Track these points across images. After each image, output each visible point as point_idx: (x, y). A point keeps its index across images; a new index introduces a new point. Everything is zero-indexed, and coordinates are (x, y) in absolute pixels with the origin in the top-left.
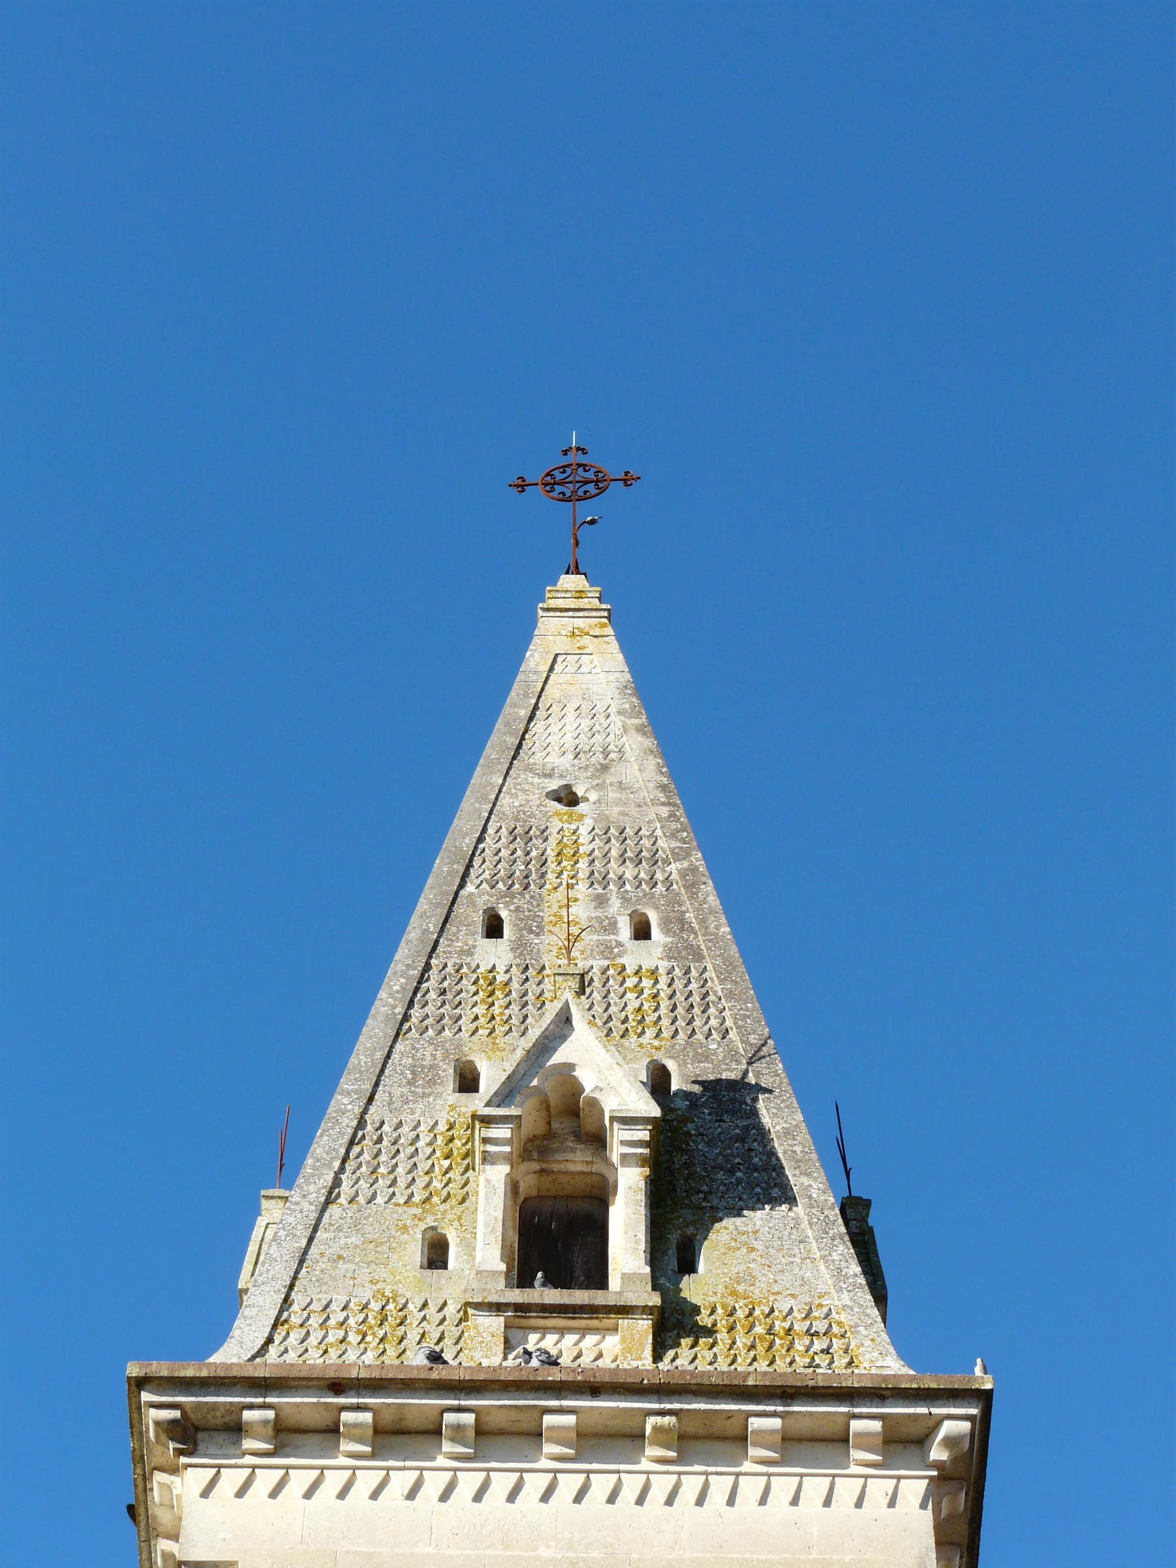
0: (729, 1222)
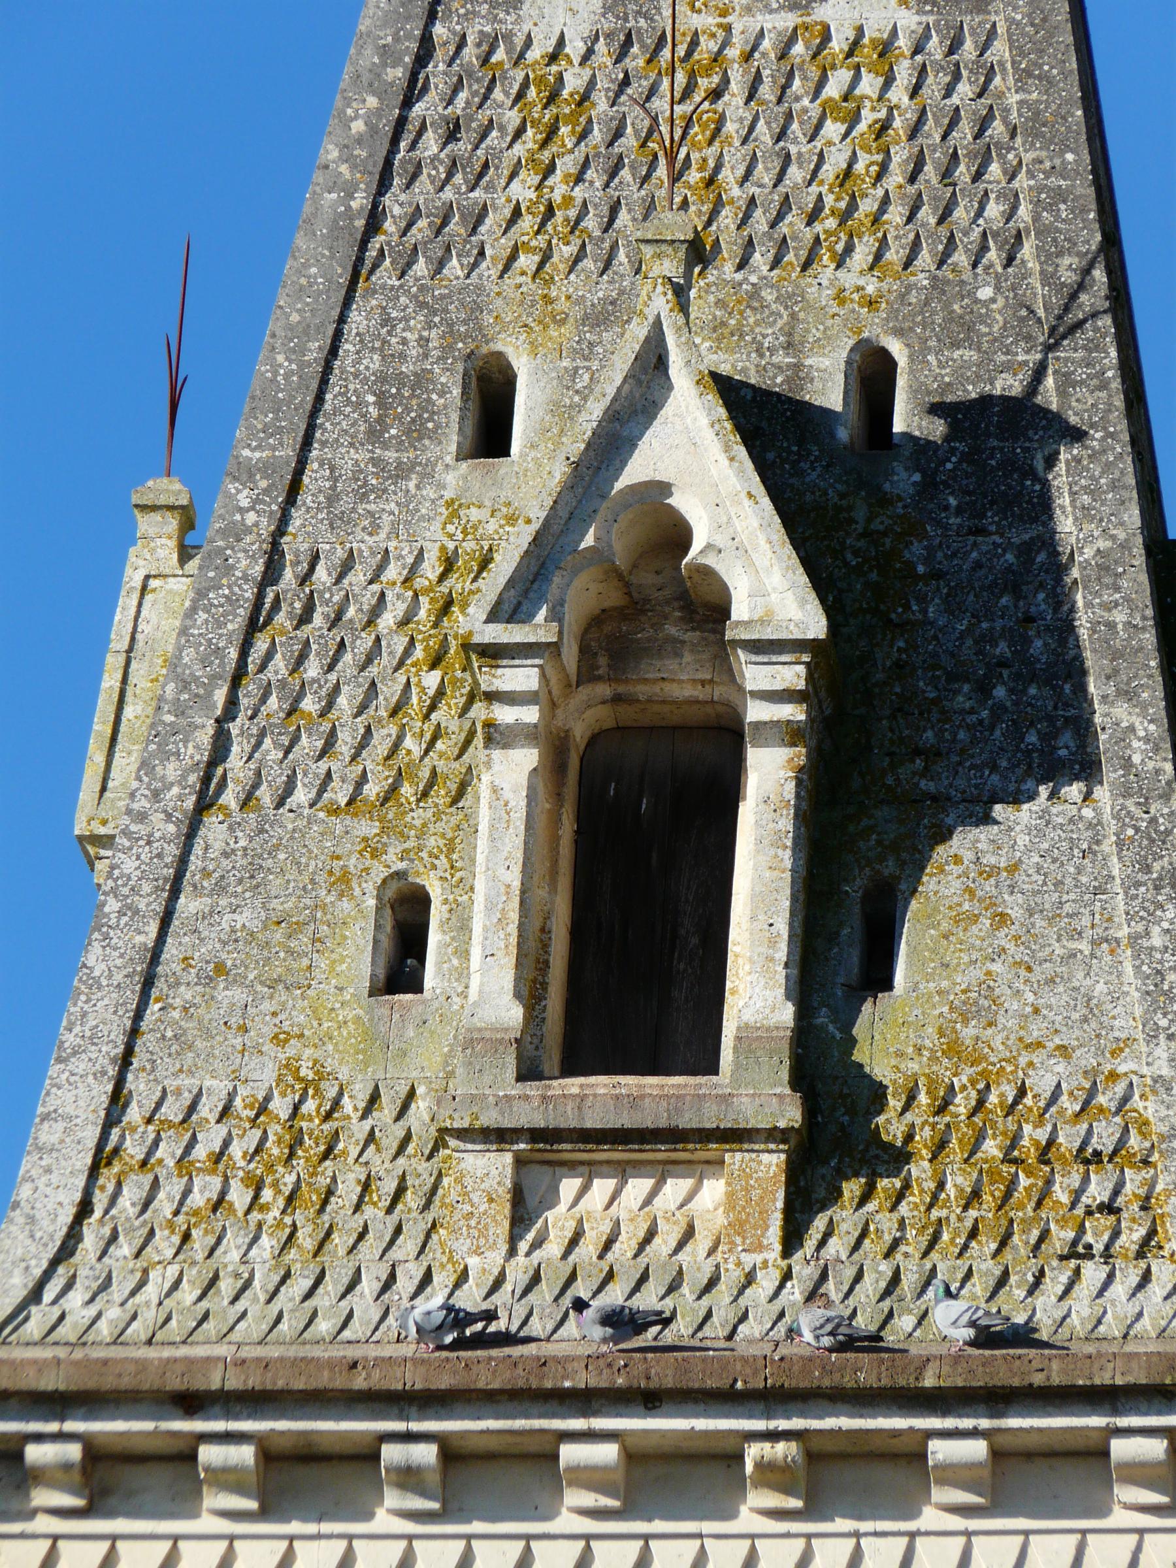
0: (966, 843)
